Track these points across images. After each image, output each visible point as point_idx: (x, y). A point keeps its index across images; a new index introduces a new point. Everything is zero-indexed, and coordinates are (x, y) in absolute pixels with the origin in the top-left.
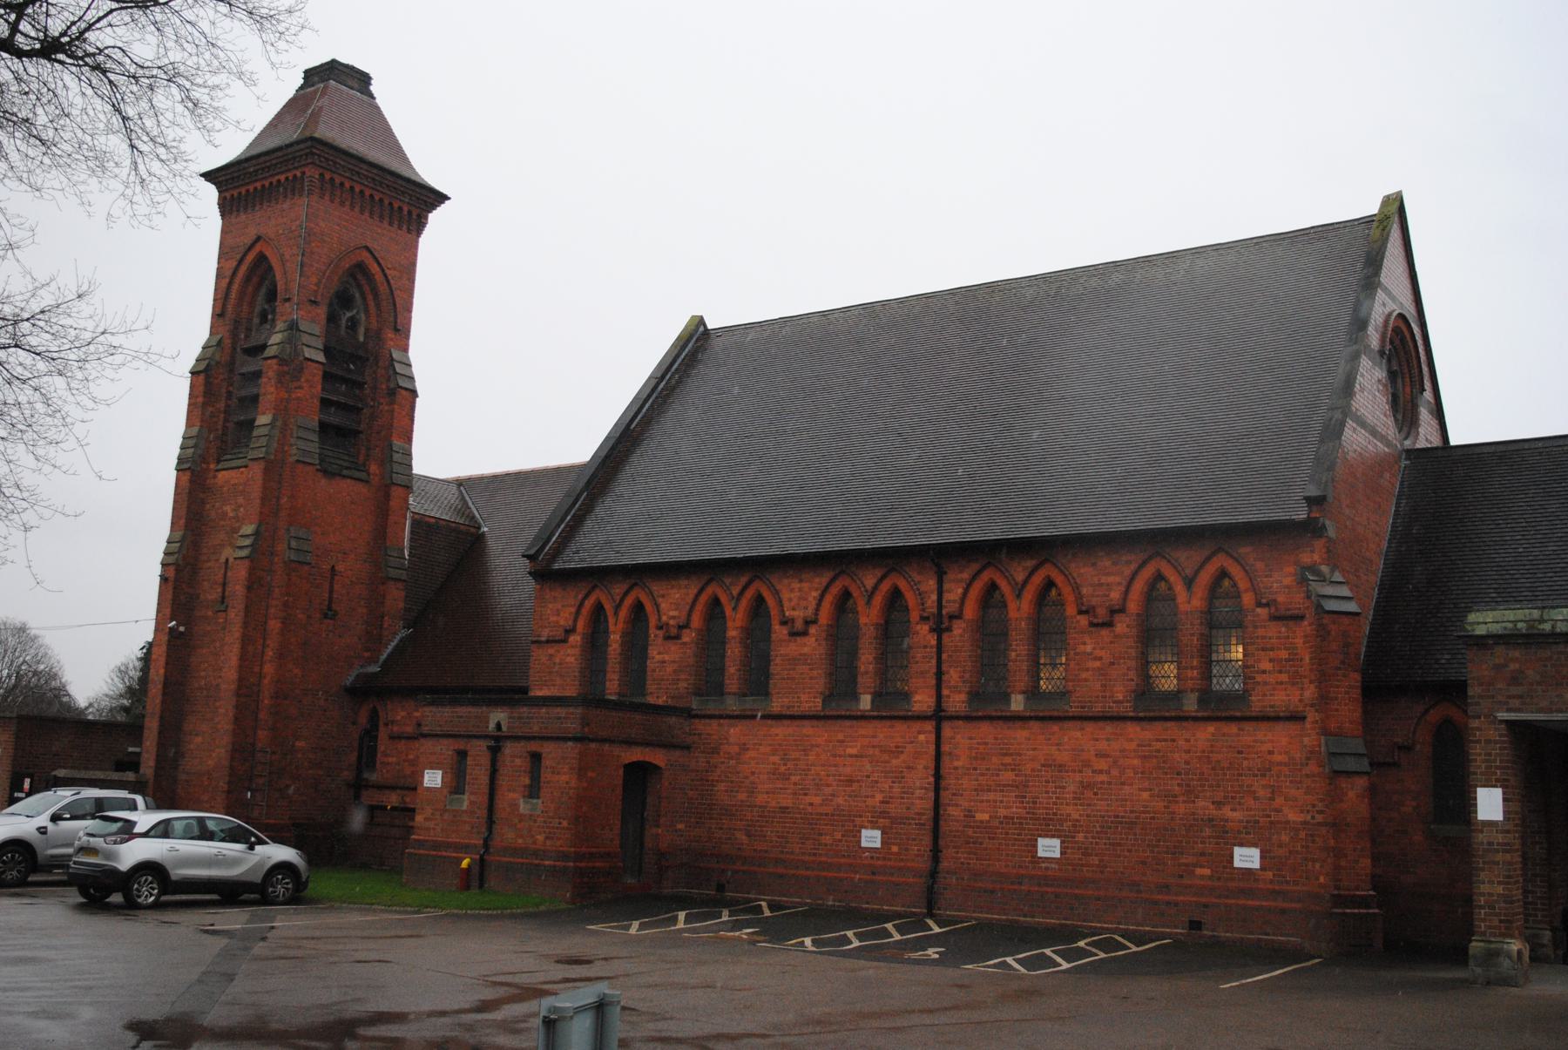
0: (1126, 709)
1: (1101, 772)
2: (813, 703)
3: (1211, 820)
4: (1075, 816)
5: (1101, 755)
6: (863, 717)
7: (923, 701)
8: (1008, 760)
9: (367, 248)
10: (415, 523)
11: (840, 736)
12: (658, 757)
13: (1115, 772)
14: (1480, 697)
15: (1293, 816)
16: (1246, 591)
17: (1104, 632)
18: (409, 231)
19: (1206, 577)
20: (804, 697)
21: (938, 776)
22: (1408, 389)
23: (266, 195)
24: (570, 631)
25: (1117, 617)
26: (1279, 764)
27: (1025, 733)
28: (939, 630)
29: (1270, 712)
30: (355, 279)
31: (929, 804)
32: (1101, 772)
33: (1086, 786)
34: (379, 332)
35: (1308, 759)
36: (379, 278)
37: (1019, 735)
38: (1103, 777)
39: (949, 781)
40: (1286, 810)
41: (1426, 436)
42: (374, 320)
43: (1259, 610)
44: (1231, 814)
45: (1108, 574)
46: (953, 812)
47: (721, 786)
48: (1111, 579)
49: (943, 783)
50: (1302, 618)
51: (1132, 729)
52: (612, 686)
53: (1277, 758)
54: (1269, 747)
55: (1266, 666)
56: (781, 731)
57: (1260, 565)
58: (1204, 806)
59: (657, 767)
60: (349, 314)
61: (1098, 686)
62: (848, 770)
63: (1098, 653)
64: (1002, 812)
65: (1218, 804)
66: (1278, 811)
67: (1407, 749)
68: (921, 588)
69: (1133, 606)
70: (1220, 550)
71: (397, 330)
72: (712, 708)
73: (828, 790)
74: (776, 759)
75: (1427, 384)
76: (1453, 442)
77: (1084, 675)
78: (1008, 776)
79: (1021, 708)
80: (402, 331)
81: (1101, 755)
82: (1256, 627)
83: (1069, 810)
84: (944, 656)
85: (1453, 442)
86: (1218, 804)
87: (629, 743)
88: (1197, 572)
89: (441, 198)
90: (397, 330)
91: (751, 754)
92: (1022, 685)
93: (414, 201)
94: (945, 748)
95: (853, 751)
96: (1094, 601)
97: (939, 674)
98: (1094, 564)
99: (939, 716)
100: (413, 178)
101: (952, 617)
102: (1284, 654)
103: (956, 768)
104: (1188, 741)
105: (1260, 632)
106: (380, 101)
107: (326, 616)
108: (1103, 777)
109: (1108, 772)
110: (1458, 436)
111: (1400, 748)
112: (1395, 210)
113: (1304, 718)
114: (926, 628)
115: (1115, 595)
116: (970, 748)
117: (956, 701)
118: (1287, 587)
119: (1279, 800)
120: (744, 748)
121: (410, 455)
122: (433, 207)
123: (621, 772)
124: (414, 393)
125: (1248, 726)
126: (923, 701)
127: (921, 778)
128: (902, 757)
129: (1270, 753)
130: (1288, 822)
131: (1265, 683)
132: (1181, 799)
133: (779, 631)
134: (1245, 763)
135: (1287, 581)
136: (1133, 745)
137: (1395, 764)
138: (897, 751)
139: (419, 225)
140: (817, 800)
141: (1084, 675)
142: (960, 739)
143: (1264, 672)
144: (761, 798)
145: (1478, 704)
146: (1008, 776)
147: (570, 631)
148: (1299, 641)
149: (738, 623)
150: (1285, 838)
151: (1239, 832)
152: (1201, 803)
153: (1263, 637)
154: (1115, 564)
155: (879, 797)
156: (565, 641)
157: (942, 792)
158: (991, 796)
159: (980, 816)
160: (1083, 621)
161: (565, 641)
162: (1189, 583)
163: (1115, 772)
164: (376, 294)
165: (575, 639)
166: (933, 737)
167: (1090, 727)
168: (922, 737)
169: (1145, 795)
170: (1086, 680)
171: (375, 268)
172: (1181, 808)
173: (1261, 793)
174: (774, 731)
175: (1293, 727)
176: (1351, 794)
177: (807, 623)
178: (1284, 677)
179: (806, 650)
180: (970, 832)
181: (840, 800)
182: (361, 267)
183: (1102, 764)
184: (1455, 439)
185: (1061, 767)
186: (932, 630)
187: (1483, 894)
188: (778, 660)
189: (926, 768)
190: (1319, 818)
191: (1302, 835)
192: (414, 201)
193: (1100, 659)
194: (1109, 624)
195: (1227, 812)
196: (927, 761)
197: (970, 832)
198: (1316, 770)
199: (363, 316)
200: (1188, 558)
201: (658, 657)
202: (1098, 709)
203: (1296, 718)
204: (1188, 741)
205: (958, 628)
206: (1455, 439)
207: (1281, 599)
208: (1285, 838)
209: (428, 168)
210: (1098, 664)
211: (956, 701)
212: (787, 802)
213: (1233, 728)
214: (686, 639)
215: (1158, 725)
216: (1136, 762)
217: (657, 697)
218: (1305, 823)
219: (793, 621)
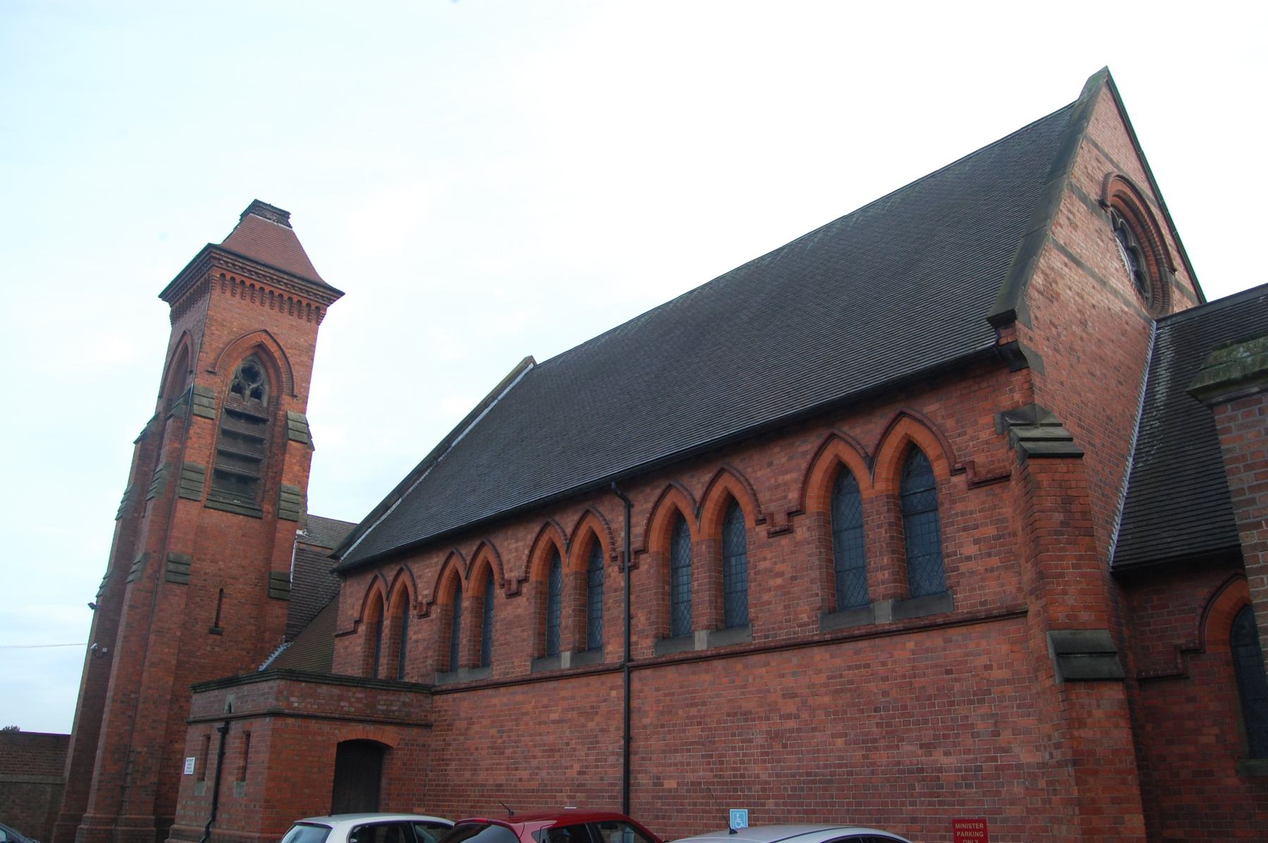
0: (813, 632)
1: (788, 717)
2: (522, 667)
3: (921, 770)
4: (764, 777)
5: (790, 695)
6: (562, 677)
7: (613, 652)
8: (694, 711)
9: (266, 331)
10: (300, 551)
11: (545, 701)
12: (388, 736)
13: (805, 715)
14: (1252, 489)
15: (1026, 756)
16: (938, 457)
17: (784, 541)
18: (309, 320)
19: (889, 451)
20: (517, 662)
21: (628, 739)
22: (1154, 269)
23: (192, 301)
24: (357, 622)
25: (797, 520)
26: (1001, 682)
27: (707, 677)
28: (629, 569)
29: (981, 611)
30: (260, 359)
31: (620, 773)
32: (788, 717)
33: (774, 736)
34: (278, 398)
35: (1036, 670)
36: (277, 354)
37: (702, 679)
38: (792, 724)
39: (638, 744)
40: (1016, 749)
41: (1180, 304)
42: (274, 389)
43: (955, 479)
44: (945, 761)
45: (786, 472)
46: (642, 780)
47: (453, 765)
48: (788, 477)
49: (633, 745)
50: (1006, 478)
51: (819, 654)
52: (383, 673)
53: (997, 674)
54: (984, 660)
55: (970, 550)
56: (499, 699)
57: (950, 423)
58: (909, 751)
59: (388, 747)
60: (254, 386)
61: (780, 609)
62: (550, 739)
63: (780, 567)
64: (690, 777)
65: (928, 747)
66: (1006, 750)
67: (1194, 652)
68: (610, 520)
69: (813, 505)
70: (902, 414)
71: (294, 396)
72: (450, 682)
73: (534, 763)
74: (493, 731)
75: (1177, 262)
76: (1209, 298)
77: (766, 597)
78: (694, 732)
79: (704, 647)
80: (301, 400)
81: (790, 695)
82: (954, 502)
83: (756, 769)
84: (633, 598)
85: (1209, 298)
86: (928, 747)
87: (345, 719)
88: (878, 447)
89: (342, 294)
90: (294, 396)
91: (476, 728)
92: (704, 621)
93: (315, 297)
94: (635, 704)
95: (554, 716)
96: (773, 507)
97: (629, 617)
98: (770, 464)
99: (629, 667)
100: (312, 278)
101: (638, 552)
102: (990, 531)
103: (645, 727)
104: (884, 664)
105: (959, 507)
106: (296, 229)
107: (212, 632)
108: (792, 724)
109: (797, 717)
110: (1212, 293)
111: (1183, 652)
112: (1103, 85)
113: (1025, 613)
114: (616, 569)
115: (793, 495)
116: (658, 701)
117: (644, 648)
118: (987, 442)
119: (1006, 735)
120: (471, 722)
121: (305, 496)
122: (331, 301)
123: (334, 750)
124: (308, 446)
125: (955, 634)
126: (613, 652)
127: (612, 743)
128: (597, 719)
129: (988, 667)
130: (1019, 766)
131: (972, 573)
132: (882, 744)
133: (499, 593)
134: (957, 685)
135: (985, 435)
136: (822, 678)
137: (1180, 677)
138: (591, 713)
139: (318, 315)
140: (525, 774)
141: (766, 597)
142: (648, 686)
143: (969, 558)
144: (482, 776)
145: (1252, 502)
146: (694, 732)
147: (357, 622)
148: (1007, 510)
149: (470, 593)
150: (1018, 789)
151: (958, 786)
152: (906, 748)
153: (963, 514)
154: (790, 459)
155: (577, 767)
156: (354, 632)
157: (632, 757)
158: (679, 757)
159: (670, 784)
160: (762, 531)
161: (354, 632)
162: (871, 461)
163: (805, 715)
164: (277, 370)
165: (362, 628)
166: (622, 692)
167: (775, 659)
168: (614, 693)
169: (840, 742)
170: (769, 603)
171: (273, 348)
172: (882, 758)
173: (981, 726)
174: (495, 701)
175: (1011, 626)
176: (1098, 714)
177: (520, 582)
178: (995, 561)
179: (520, 611)
180: (659, 804)
181: (543, 773)
182: (261, 346)
183: (790, 707)
184: (1211, 296)
185: (746, 715)
186: (621, 570)
187: (613, 766)
188: (498, 625)
189: (617, 729)
190: (1058, 754)
191: (1042, 784)
192: (315, 297)
193: (781, 574)
194: (787, 531)
195: (939, 758)
196: (618, 722)
197: (659, 804)
198: (1048, 683)
199: (267, 387)
200: (866, 431)
201: (414, 637)
202: (782, 636)
203: (1015, 614)
204: (884, 664)
205: (646, 562)
206: (1211, 296)
207: (980, 459)
208: (1018, 789)
209: (328, 273)
210: (779, 581)
211: (644, 648)
212: (502, 779)
213: (935, 640)
214: (433, 616)
215: (848, 647)
216: (827, 699)
217: (411, 677)
218: (1044, 765)
219: (509, 582)
